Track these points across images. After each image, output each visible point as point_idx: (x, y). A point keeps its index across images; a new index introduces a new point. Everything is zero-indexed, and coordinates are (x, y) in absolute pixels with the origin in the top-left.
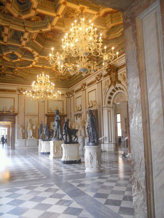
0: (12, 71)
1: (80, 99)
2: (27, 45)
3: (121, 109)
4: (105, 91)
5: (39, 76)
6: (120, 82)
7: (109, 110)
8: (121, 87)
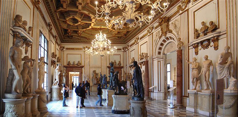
0: (77, 33)
1: (133, 52)
2: (83, 8)
3: (171, 59)
4: (156, 43)
5: (98, 36)
6: (171, 32)
7: (158, 61)
8: (172, 36)
